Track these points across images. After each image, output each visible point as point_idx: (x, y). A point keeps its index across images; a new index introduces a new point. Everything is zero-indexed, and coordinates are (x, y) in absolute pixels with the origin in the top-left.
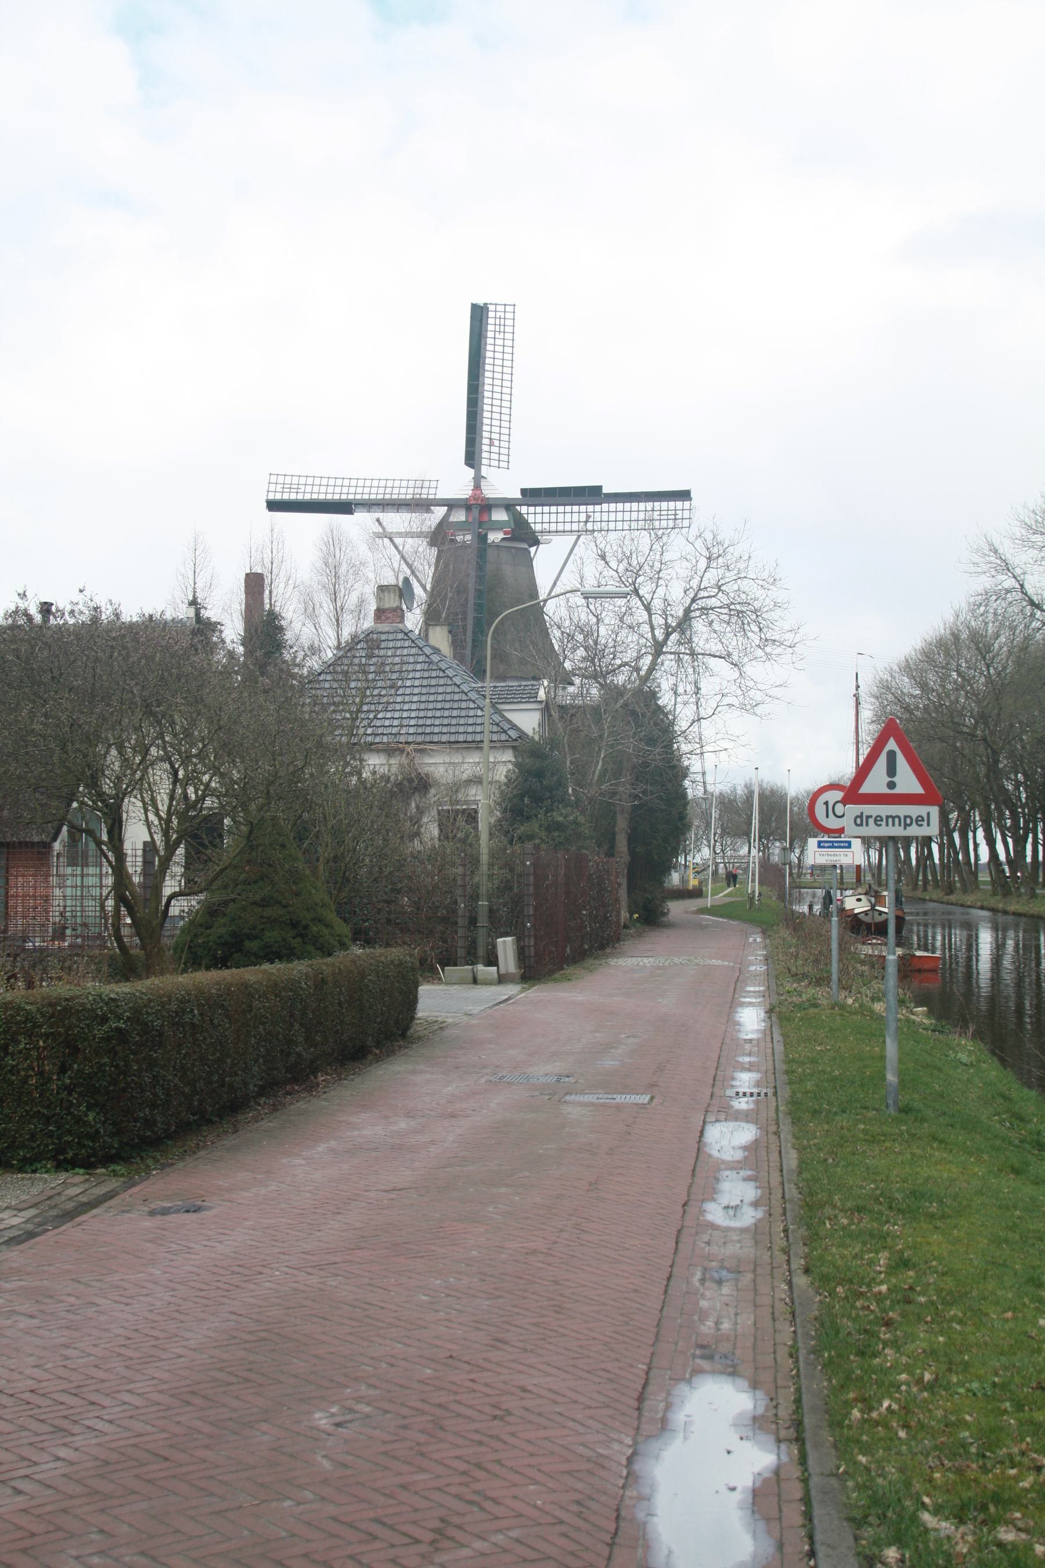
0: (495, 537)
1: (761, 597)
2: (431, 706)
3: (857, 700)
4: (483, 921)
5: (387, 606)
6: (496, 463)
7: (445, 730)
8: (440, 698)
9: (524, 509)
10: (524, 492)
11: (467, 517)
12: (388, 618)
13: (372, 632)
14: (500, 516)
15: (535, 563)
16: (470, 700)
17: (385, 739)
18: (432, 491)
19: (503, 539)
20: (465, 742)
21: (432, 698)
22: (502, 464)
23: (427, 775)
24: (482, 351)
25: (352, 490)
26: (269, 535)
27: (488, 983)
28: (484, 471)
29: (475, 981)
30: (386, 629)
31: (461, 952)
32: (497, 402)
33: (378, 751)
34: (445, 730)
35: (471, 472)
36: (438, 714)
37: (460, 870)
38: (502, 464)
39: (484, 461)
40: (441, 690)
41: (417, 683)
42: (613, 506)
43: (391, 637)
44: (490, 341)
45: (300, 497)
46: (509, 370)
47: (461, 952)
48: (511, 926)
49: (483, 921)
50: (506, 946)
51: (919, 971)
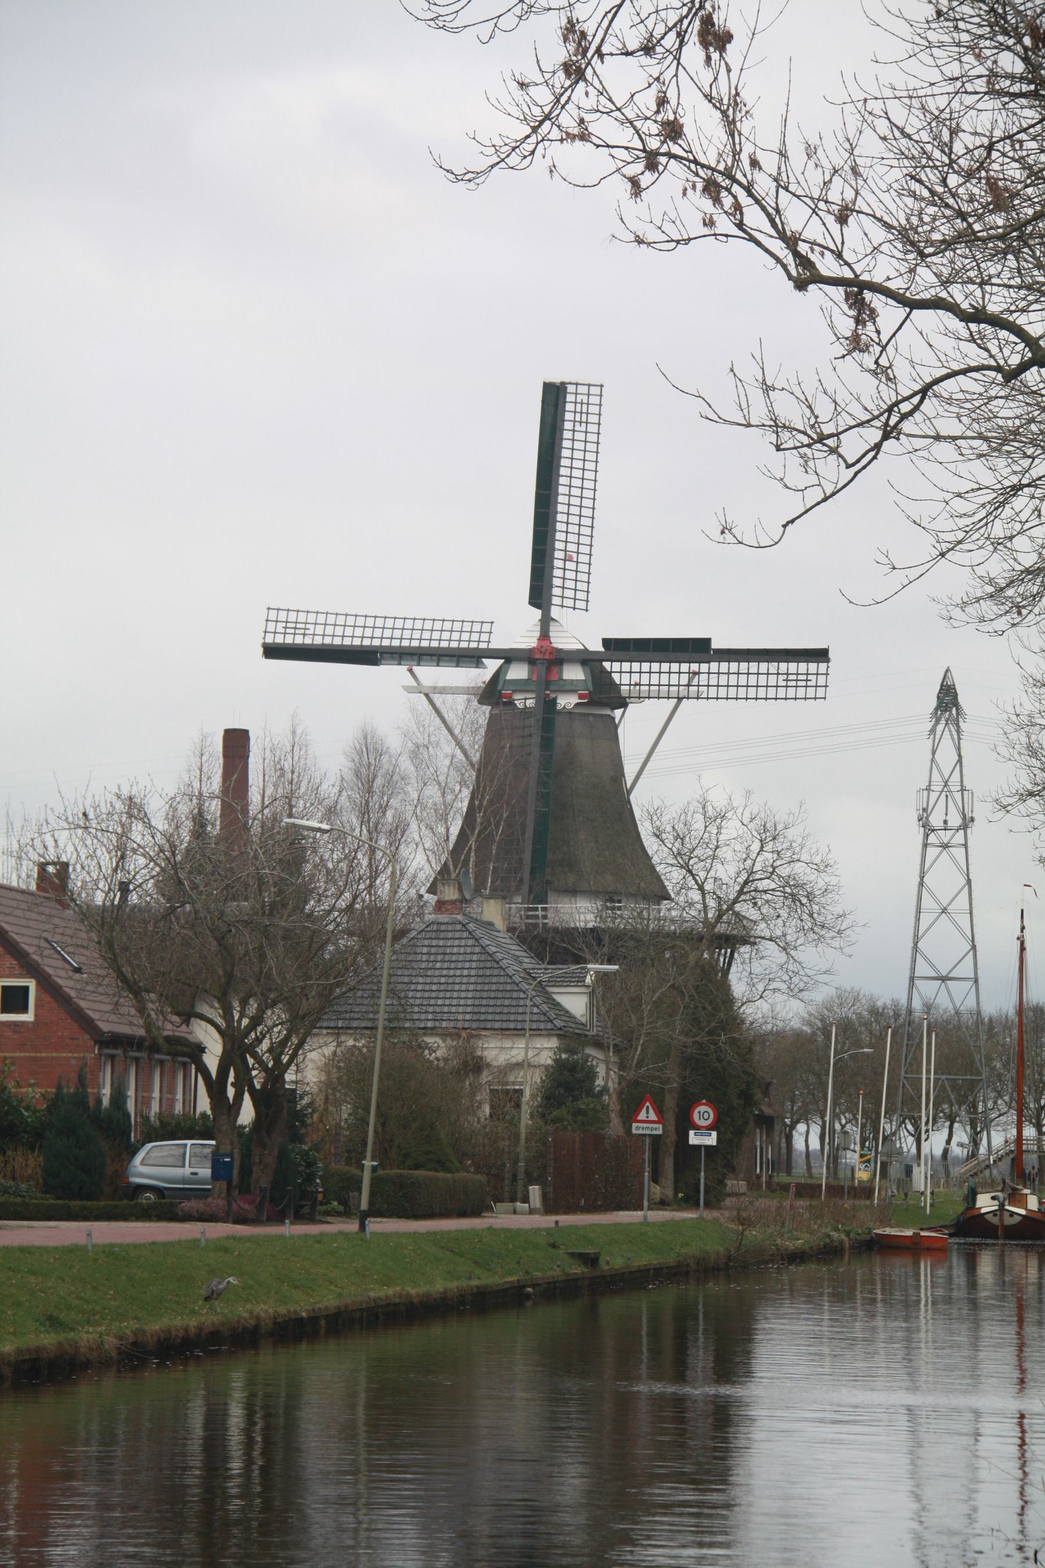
0: (567, 701)
1: (818, 882)
2: (485, 995)
3: (1022, 943)
4: (521, 1175)
5: (447, 898)
6: (570, 603)
7: (497, 1017)
8: (494, 987)
9: (607, 665)
10: (607, 642)
11: (530, 673)
12: (447, 910)
13: (433, 923)
14: (574, 673)
15: (620, 731)
16: (521, 990)
17: (444, 1024)
18: (485, 637)
19: (577, 704)
20: (515, 1029)
21: (486, 987)
22: (580, 604)
23: (481, 1058)
24: (557, 448)
25: (378, 633)
26: (290, 737)
27: (522, 1213)
28: (555, 612)
29: (515, 1212)
30: (446, 920)
31: (506, 1195)
32: (575, 501)
33: (437, 1035)
34: (497, 1017)
35: (537, 613)
36: (492, 1002)
37: (507, 1143)
38: (579, 604)
39: (556, 600)
40: (494, 980)
41: (473, 972)
42: (724, 666)
43: (450, 928)
44: (567, 435)
45: (308, 641)
46: (589, 503)
47: (506, 1195)
48: (540, 1180)
49: (521, 1175)
50: (535, 1191)
51: (928, 1249)
